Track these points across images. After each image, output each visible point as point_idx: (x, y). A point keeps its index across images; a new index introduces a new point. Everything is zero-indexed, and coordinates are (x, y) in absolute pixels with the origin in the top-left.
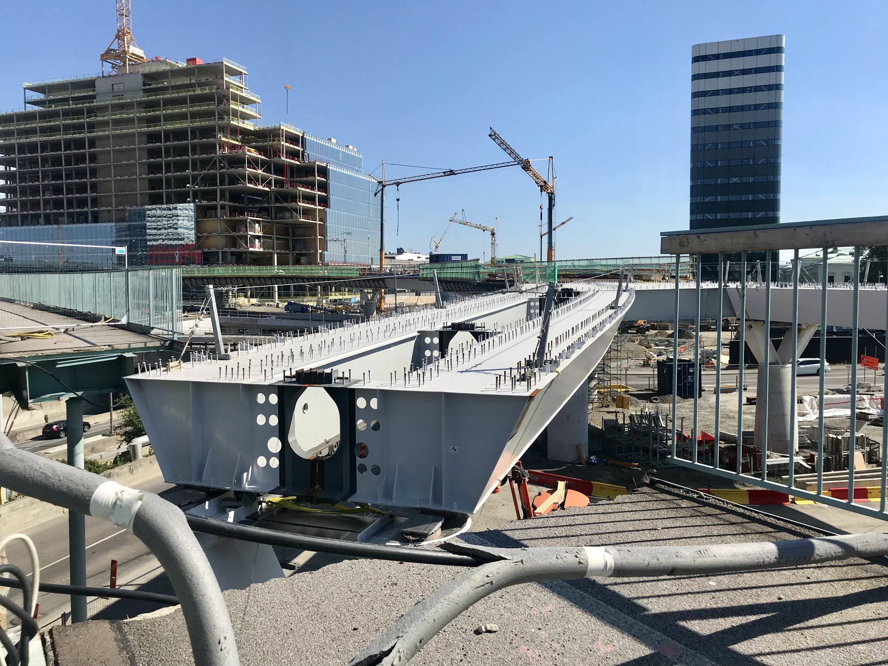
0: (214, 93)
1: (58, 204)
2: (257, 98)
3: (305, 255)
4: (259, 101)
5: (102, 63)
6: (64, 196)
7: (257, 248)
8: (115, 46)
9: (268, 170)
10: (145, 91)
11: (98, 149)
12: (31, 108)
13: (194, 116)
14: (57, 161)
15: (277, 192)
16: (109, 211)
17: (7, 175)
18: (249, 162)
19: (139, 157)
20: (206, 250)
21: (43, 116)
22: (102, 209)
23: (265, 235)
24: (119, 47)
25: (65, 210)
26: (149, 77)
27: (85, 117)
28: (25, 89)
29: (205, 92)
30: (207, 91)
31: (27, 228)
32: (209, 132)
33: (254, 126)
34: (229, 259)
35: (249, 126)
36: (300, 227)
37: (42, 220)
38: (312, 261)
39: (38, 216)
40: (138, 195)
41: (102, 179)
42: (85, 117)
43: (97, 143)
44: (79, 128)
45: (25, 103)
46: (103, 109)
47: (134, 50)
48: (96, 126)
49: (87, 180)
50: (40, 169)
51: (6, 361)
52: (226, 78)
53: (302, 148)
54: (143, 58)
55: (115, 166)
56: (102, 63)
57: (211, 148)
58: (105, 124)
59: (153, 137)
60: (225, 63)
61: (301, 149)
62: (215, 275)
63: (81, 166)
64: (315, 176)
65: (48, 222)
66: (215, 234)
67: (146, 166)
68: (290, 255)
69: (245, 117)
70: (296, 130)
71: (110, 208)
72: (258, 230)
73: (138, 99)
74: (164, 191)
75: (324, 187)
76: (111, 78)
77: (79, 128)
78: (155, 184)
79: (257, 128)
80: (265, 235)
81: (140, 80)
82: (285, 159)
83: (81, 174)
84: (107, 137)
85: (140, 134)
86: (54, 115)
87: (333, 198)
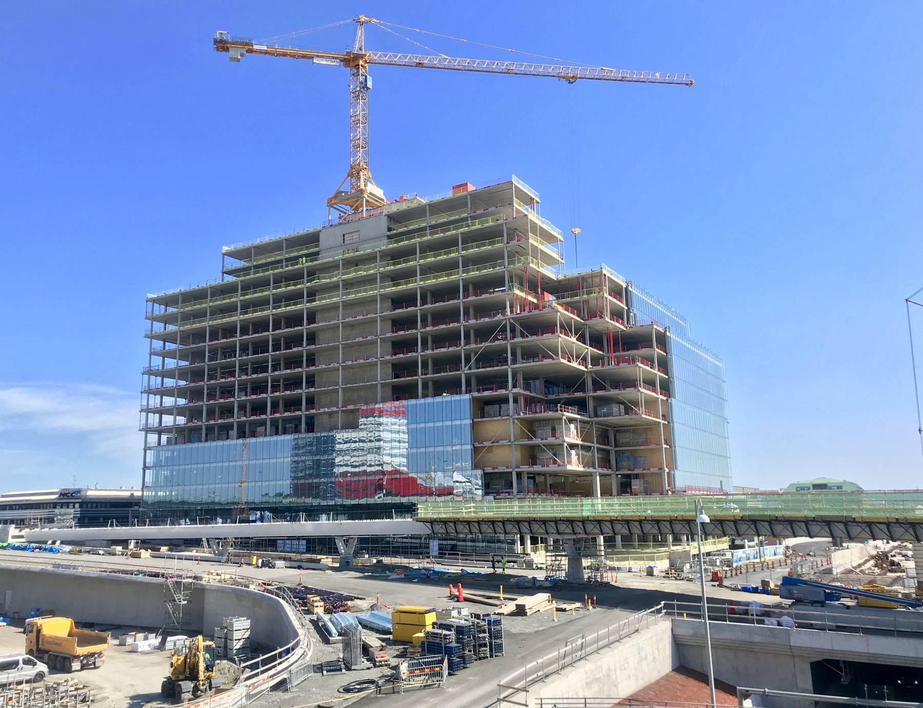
0: (502, 224)
1: (259, 408)
2: (559, 234)
3: (637, 476)
4: (560, 238)
5: (329, 209)
6: (268, 396)
7: (574, 465)
8: (346, 187)
9: (581, 339)
10: (389, 237)
11: (320, 324)
12: (230, 279)
13: (469, 262)
14: (261, 347)
15: (596, 372)
16: (330, 414)
17: (191, 391)
18: (562, 327)
19: (381, 330)
20: (489, 470)
21: (247, 287)
22: (322, 410)
23: (586, 444)
24: (351, 188)
25: (268, 416)
26: (395, 218)
27: (305, 281)
28: (224, 254)
29: (487, 225)
30: (491, 224)
31: (214, 444)
32: (497, 282)
33: (557, 274)
34: (526, 484)
35: (550, 272)
36: (625, 431)
37: (234, 433)
38: (653, 488)
39: (230, 427)
40: (379, 387)
41: (324, 366)
42: (305, 281)
43: (318, 317)
44: (295, 297)
45: (224, 273)
46: (332, 267)
47: (373, 189)
48: (317, 293)
49: (303, 370)
50: (237, 360)
51: (156, 555)
52: (517, 205)
53: (627, 305)
54: (382, 200)
55: (345, 347)
56: (329, 209)
57: (499, 307)
58: (334, 287)
59: (398, 301)
60: (515, 182)
61: (626, 308)
62: (585, 514)
63: (295, 349)
64: (651, 347)
65: (242, 435)
66: (505, 442)
67: (390, 344)
68: (614, 476)
69: (547, 259)
70: (618, 278)
71: (335, 409)
72: (572, 436)
73: (384, 248)
74: (419, 378)
75: (664, 365)
76: (342, 226)
77: (295, 297)
78: (399, 369)
79: (561, 277)
80: (586, 444)
81: (384, 223)
82: (609, 320)
83: (294, 362)
84: (334, 307)
85: (384, 297)
86: (263, 284)
87: (678, 386)
